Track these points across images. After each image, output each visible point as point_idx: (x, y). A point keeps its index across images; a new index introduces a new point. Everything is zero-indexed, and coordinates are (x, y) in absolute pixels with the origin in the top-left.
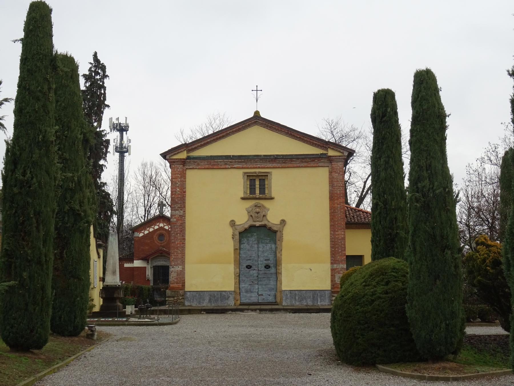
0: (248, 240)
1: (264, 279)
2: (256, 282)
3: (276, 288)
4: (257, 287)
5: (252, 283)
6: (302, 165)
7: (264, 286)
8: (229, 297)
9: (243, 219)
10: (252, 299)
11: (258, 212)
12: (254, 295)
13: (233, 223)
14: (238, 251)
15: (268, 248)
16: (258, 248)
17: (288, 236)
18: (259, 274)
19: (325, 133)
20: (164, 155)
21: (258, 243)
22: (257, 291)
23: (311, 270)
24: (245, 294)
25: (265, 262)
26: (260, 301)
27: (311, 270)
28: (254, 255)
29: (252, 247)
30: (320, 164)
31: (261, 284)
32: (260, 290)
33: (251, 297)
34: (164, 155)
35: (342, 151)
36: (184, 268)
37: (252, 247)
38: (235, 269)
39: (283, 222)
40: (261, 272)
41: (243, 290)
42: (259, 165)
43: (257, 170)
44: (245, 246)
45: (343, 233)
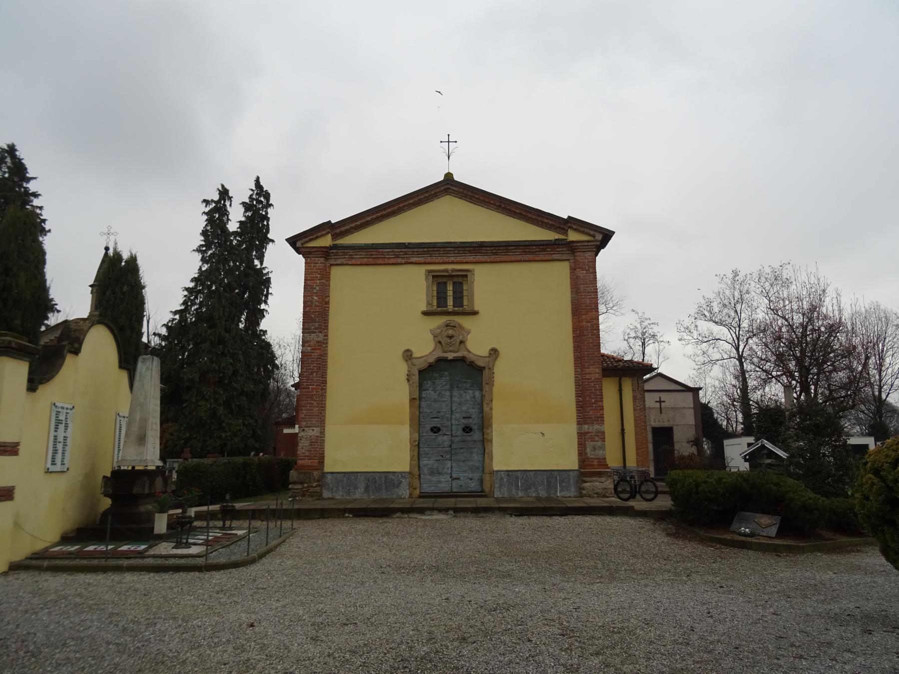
0: (434, 383)
1: (462, 451)
2: (448, 456)
3: (483, 467)
6: (525, 257)
7: (461, 464)
9: (425, 348)
11: (450, 337)
12: (445, 478)
13: (408, 355)
15: (468, 397)
16: (451, 397)
17: (504, 376)
18: (452, 442)
22: (449, 471)
23: (543, 434)
24: (428, 477)
25: (463, 421)
29: (440, 395)
33: (440, 482)
35: (592, 233)
37: (440, 395)
38: (411, 434)
39: (494, 352)
42: (452, 259)
43: (450, 267)
44: (430, 393)
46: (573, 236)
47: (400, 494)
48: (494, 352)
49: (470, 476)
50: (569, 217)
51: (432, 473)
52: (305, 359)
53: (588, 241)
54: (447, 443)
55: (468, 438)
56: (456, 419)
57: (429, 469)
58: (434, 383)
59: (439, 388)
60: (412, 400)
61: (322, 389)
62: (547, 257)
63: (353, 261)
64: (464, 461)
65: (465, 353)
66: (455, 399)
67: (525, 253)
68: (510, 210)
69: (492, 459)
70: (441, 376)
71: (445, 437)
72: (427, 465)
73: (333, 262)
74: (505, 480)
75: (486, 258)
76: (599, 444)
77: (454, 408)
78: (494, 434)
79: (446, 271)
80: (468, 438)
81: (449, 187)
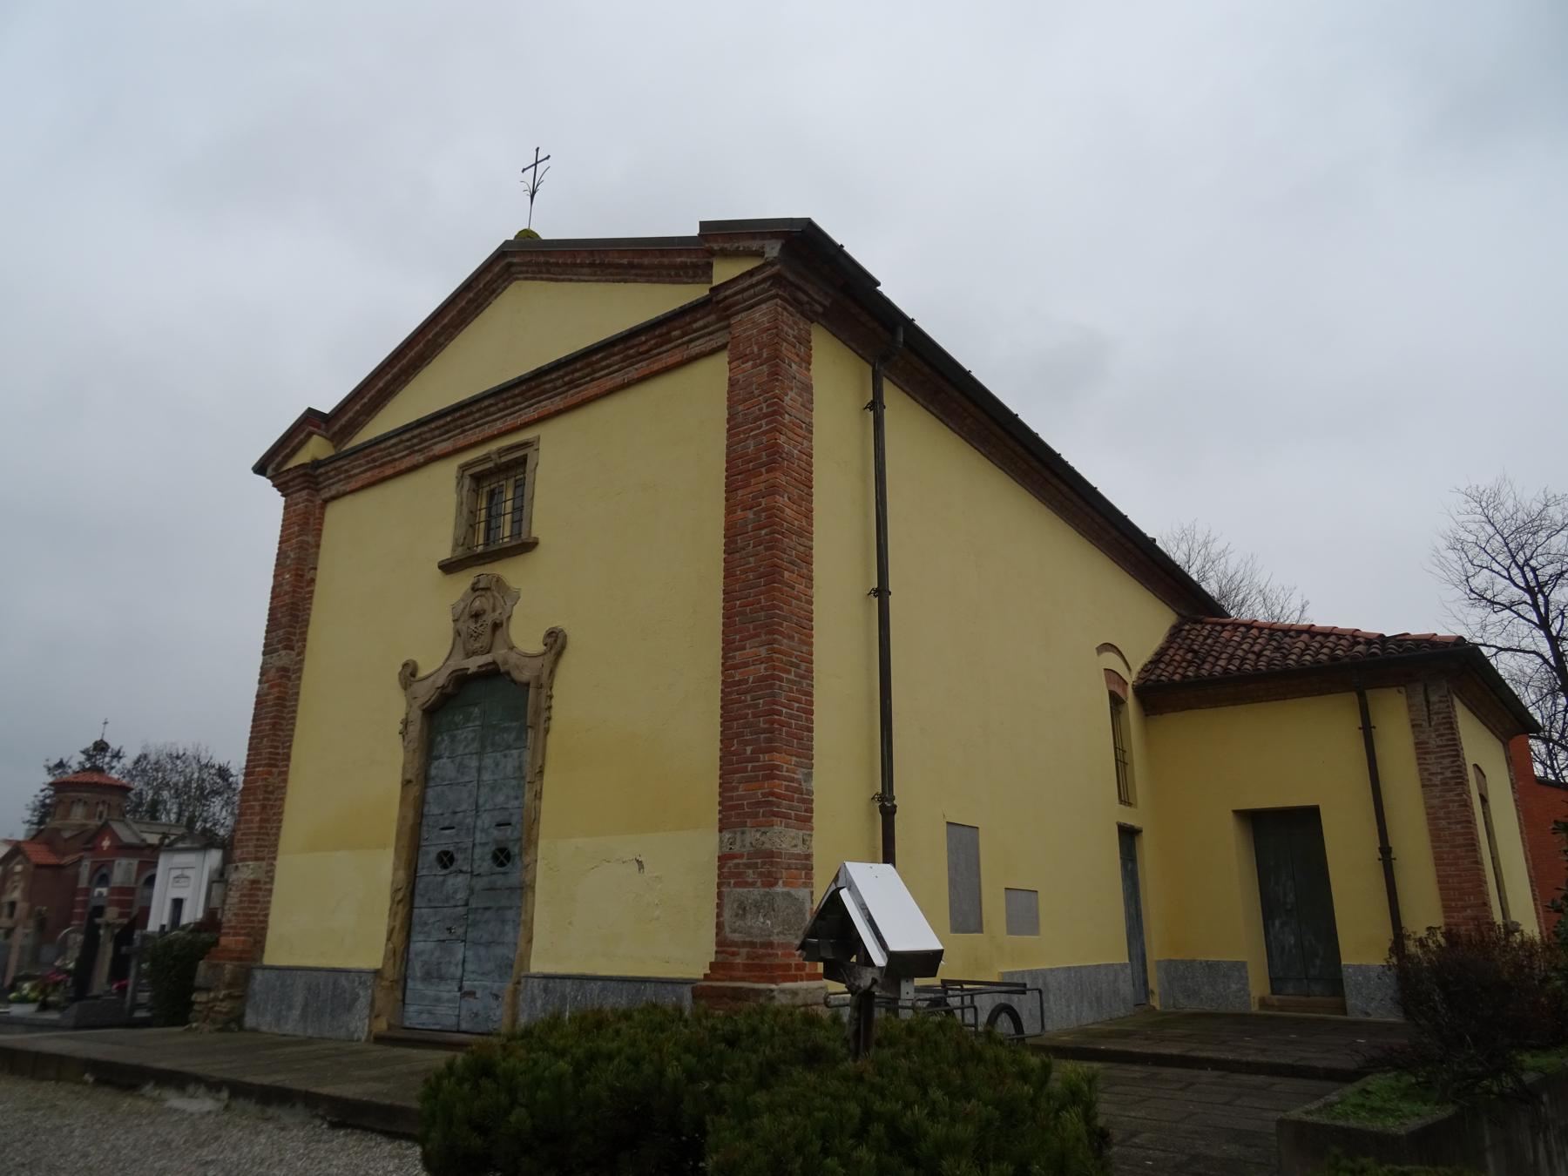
0: (453, 739)
1: (488, 914)
2: (460, 931)
3: (512, 967)
4: (460, 956)
5: (446, 935)
6: (633, 373)
7: (482, 951)
8: (356, 998)
9: (435, 655)
10: (442, 1010)
11: (482, 621)
12: (448, 991)
13: (409, 673)
14: (419, 784)
15: (510, 768)
16: (479, 770)
17: (574, 701)
18: (472, 891)
19: (1472, 527)
20: (260, 469)
21: (480, 754)
22: (459, 973)
23: (640, 863)
24: (420, 986)
25: (496, 833)
26: (464, 1026)
27: (640, 863)
28: (464, 807)
29: (461, 768)
30: (695, 348)
31: (474, 943)
32: (469, 967)
33: (438, 1000)
34: (260, 469)
35: (755, 245)
36: (270, 873)
37: (461, 768)
38: (395, 870)
39: (556, 642)
40: (480, 884)
41: (417, 969)
42: (499, 425)
43: (494, 446)
44: (444, 767)
45: (763, 652)
46: (723, 272)
47: (352, 1027)
48: (556, 642)
49: (496, 986)
50: (704, 225)
51: (427, 977)
52: (1453, 749)
53: (750, 273)
54: (461, 896)
55: (500, 881)
56: (483, 830)
57: (425, 963)
58: (453, 739)
59: (460, 750)
60: (406, 783)
61: (280, 773)
62: (677, 356)
63: (353, 485)
64: (489, 944)
65: (499, 654)
66: (486, 776)
67: (629, 361)
68: (610, 265)
69: (530, 941)
70: (467, 720)
71: (461, 878)
72: (422, 952)
73: (326, 494)
74: (539, 1003)
75: (558, 403)
76: (756, 893)
77: (481, 801)
78: (541, 867)
79: (487, 458)
80: (500, 881)
81: (524, 260)
